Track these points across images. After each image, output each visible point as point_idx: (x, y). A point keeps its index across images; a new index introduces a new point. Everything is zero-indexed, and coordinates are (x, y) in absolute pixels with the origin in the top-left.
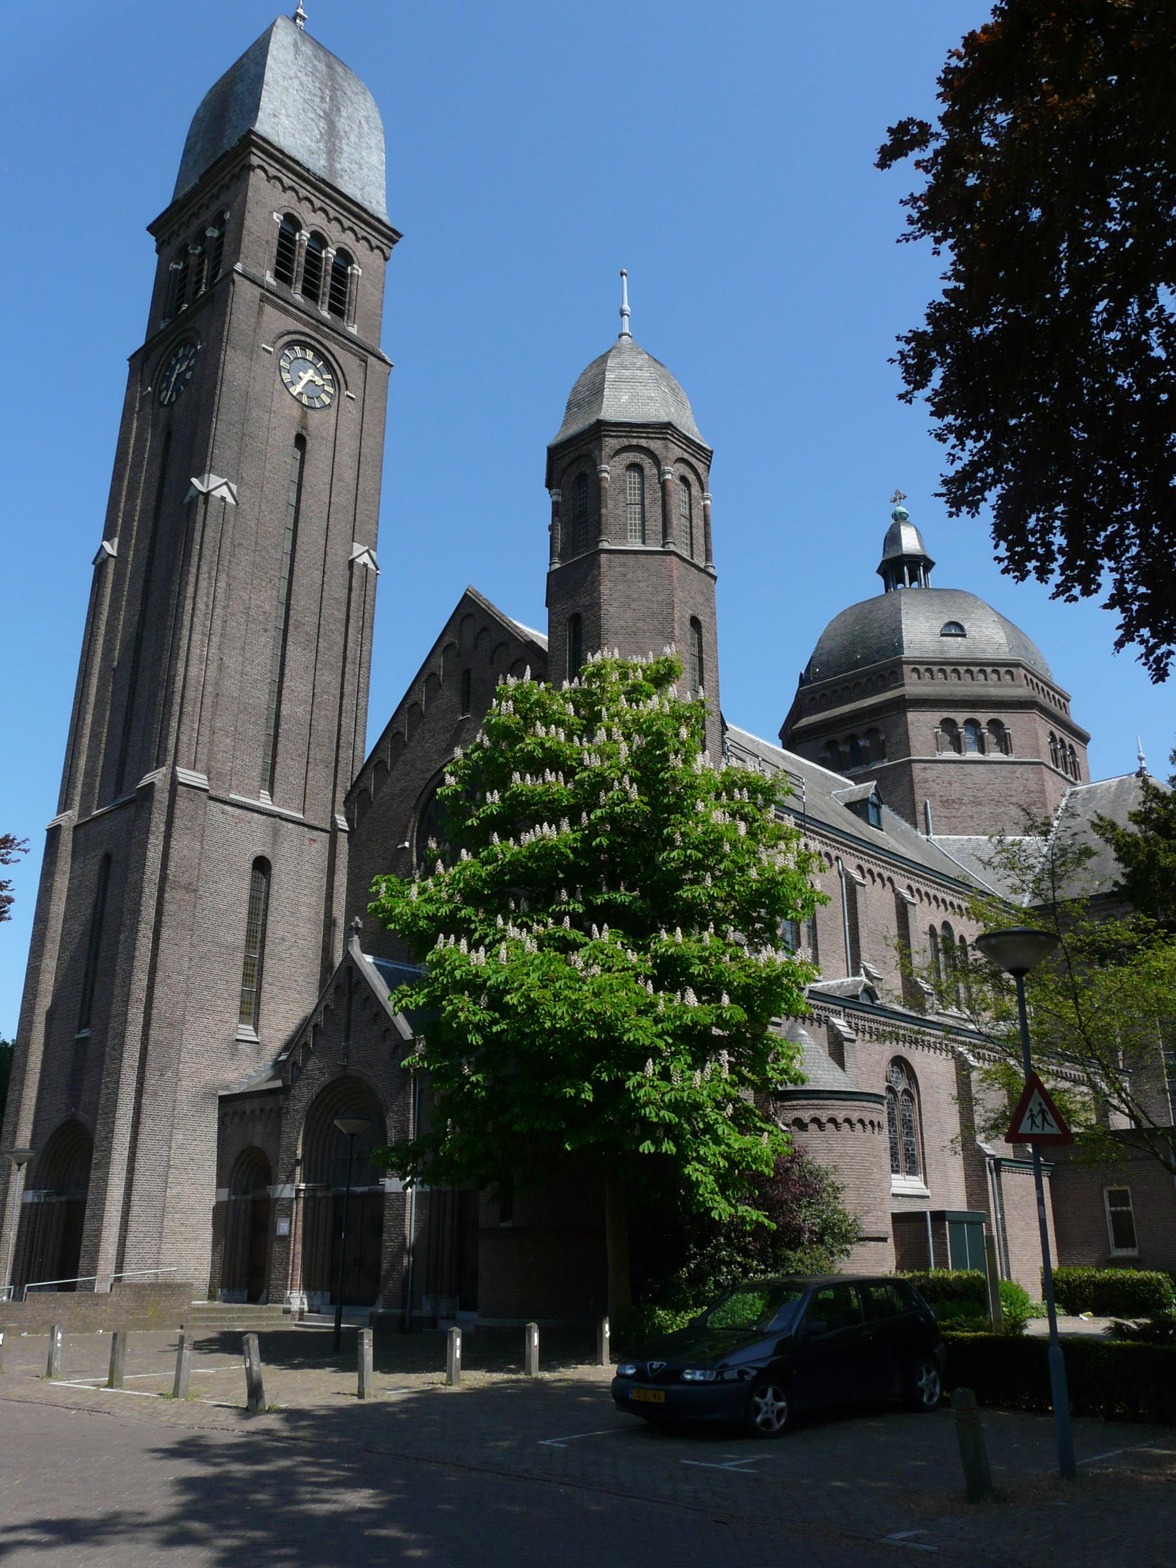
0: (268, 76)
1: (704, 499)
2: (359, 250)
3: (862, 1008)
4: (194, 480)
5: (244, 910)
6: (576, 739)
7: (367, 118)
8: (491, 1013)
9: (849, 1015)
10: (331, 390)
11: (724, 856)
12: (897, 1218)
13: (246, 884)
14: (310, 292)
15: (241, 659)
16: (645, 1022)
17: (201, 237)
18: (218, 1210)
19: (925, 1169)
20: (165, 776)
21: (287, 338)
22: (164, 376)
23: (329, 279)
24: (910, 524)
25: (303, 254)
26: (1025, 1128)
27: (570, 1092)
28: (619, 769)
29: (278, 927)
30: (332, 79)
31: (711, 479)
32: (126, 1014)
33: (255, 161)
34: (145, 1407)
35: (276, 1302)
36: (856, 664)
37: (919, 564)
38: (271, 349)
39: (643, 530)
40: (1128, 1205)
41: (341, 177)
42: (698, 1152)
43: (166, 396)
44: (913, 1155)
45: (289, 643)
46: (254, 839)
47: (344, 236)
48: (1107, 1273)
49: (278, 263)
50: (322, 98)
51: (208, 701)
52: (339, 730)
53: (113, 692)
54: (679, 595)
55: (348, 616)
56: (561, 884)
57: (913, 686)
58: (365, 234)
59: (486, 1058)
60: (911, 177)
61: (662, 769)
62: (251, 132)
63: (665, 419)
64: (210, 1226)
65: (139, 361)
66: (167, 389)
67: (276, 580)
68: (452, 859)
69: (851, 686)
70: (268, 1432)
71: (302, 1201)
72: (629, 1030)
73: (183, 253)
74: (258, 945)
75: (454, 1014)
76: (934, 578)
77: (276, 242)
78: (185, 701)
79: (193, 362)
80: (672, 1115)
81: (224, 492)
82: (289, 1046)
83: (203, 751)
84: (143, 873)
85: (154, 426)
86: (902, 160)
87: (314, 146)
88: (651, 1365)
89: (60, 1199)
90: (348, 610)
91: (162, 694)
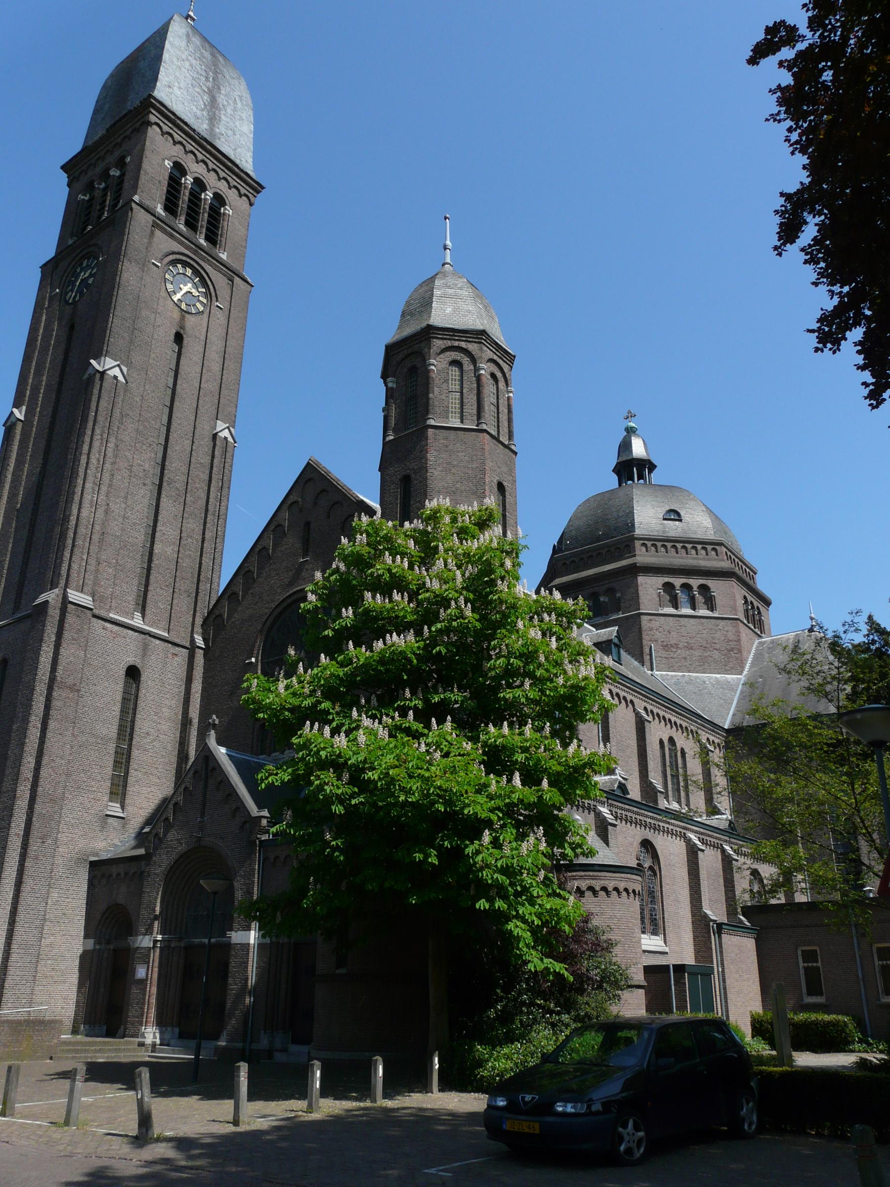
0: (166, 56)
2: (231, 195)
3: (618, 798)
4: (92, 361)
5: (117, 708)
6: (416, 568)
7: (241, 97)
8: (351, 787)
9: (611, 805)
10: (205, 301)
11: (540, 665)
12: (648, 970)
13: (120, 687)
14: (191, 224)
15: (124, 506)
16: (481, 799)
18: (85, 958)
19: (664, 930)
20: (58, 596)
21: (171, 257)
22: (70, 281)
23: (206, 215)
24: (638, 436)
25: (187, 193)
27: (419, 856)
28: (456, 591)
29: (143, 724)
30: (215, 65)
31: (515, 375)
32: (16, 791)
33: (153, 118)
34: (41, 1136)
36: (598, 539)
37: (645, 466)
38: (159, 264)
39: (462, 412)
40: (817, 962)
41: (219, 139)
42: (517, 912)
43: (71, 296)
44: (655, 919)
46: (127, 651)
48: (802, 1016)
50: (207, 79)
51: (96, 537)
52: (200, 567)
54: (489, 464)
55: (210, 477)
56: (402, 685)
57: (642, 557)
58: (236, 184)
59: (343, 826)
60: (774, 73)
61: (491, 593)
62: (150, 96)
63: (481, 328)
64: (76, 970)
65: (49, 269)
66: (72, 291)
67: (155, 445)
68: (312, 662)
69: (613, 550)
70: (166, 1161)
71: (158, 950)
72: (469, 805)
73: (90, 187)
74: (127, 738)
75: (320, 788)
76: (656, 477)
77: (166, 183)
79: (95, 271)
80: (504, 878)
81: (116, 372)
82: (149, 821)
83: (90, 577)
84: (36, 674)
85: (60, 320)
86: (771, 57)
88: (523, 1098)
90: (211, 473)
91: (58, 529)
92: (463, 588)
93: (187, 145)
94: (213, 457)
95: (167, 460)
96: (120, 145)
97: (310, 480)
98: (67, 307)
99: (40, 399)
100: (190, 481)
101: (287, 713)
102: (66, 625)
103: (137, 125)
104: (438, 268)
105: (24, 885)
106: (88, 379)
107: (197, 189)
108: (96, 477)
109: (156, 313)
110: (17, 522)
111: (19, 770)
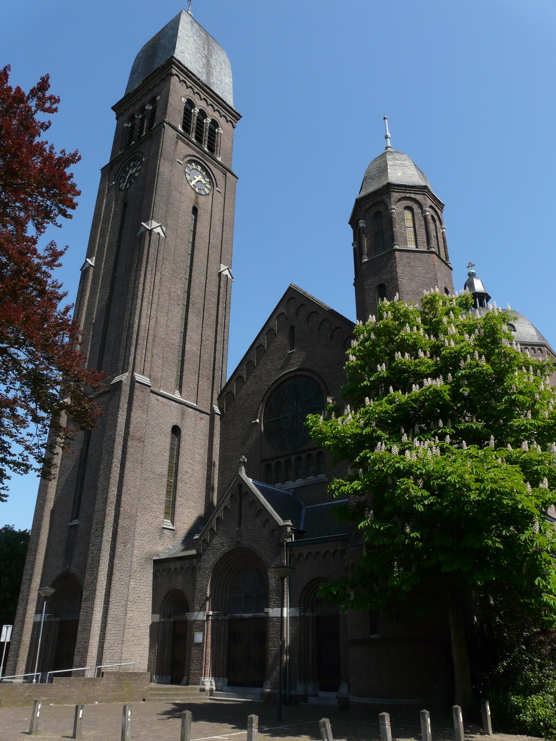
0: (179, 34)
1: (442, 229)
2: (221, 121)
5: (167, 455)
7: (224, 61)
10: (209, 187)
13: (168, 440)
14: (199, 138)
15: (166, 318)
18: (153, 627)
21: (189, 158)
23: (207, 133)
24: (477, 278)
29: (183, 466)
30: (209, 41)
33: (174, 72)
35: (194, 684)
43: (123, 186)
45: (189, 312)
46: (171, 416)
50: (204, 48)
51: (150, 338)
53: (93, 336)
58: (224, 114)
62: (173, 57)
64: (148, 637)
65: (106, 171)
66: (124, 182)
67: (184, 279)
71: (210, 622)
78: (139, 337)
79: (140, 168)
81: (159, 230)
83: (148, 365)
84: (116, 430)
85: (116, 201)
87: (200, 70)
89: (56, 620)
90: (219, 298)
92: (475, 345)
93: (195, 89)
94: (219, 287)
95: (191, 289)
98: (121, 193)
99: (105, 252)
100: (206, 303)
101: (349, 440)
102: (135, 397)
103: (164, 76)
104: (383, 151)
105: (114, 576)
106: (140, 235)
107: (201, 117)
108: (149, 298)
109: (181, 193)
110: (93, 331)
111: (107, 496)
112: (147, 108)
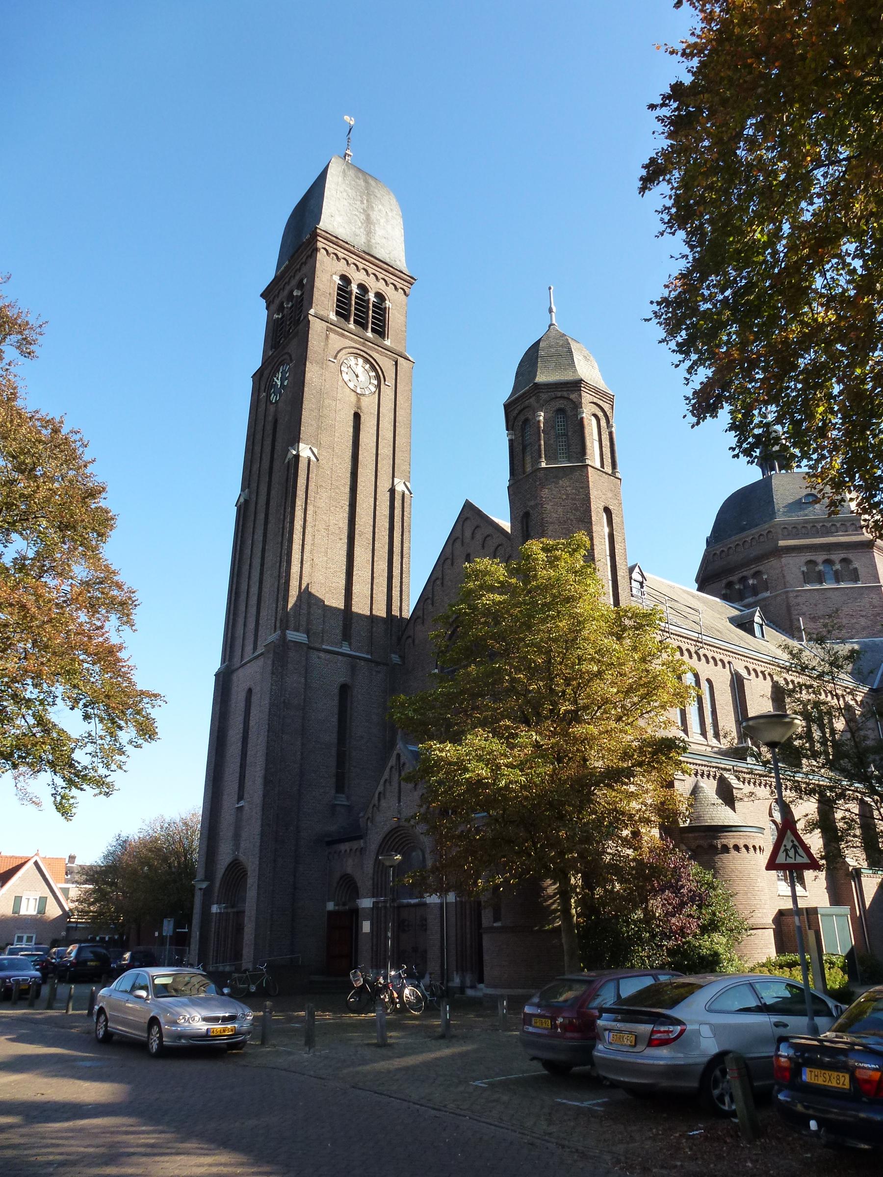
17: (290, 296)
26: (781, 859)
47: (379, 284)
49: (338, 306)
50: (362, 202)
60: (662, 193)
69: (741, 543)
73: (281, 309)
96: (299, 270)
97: (467, 519)
109: (335, 400)
112: (295, 294)
